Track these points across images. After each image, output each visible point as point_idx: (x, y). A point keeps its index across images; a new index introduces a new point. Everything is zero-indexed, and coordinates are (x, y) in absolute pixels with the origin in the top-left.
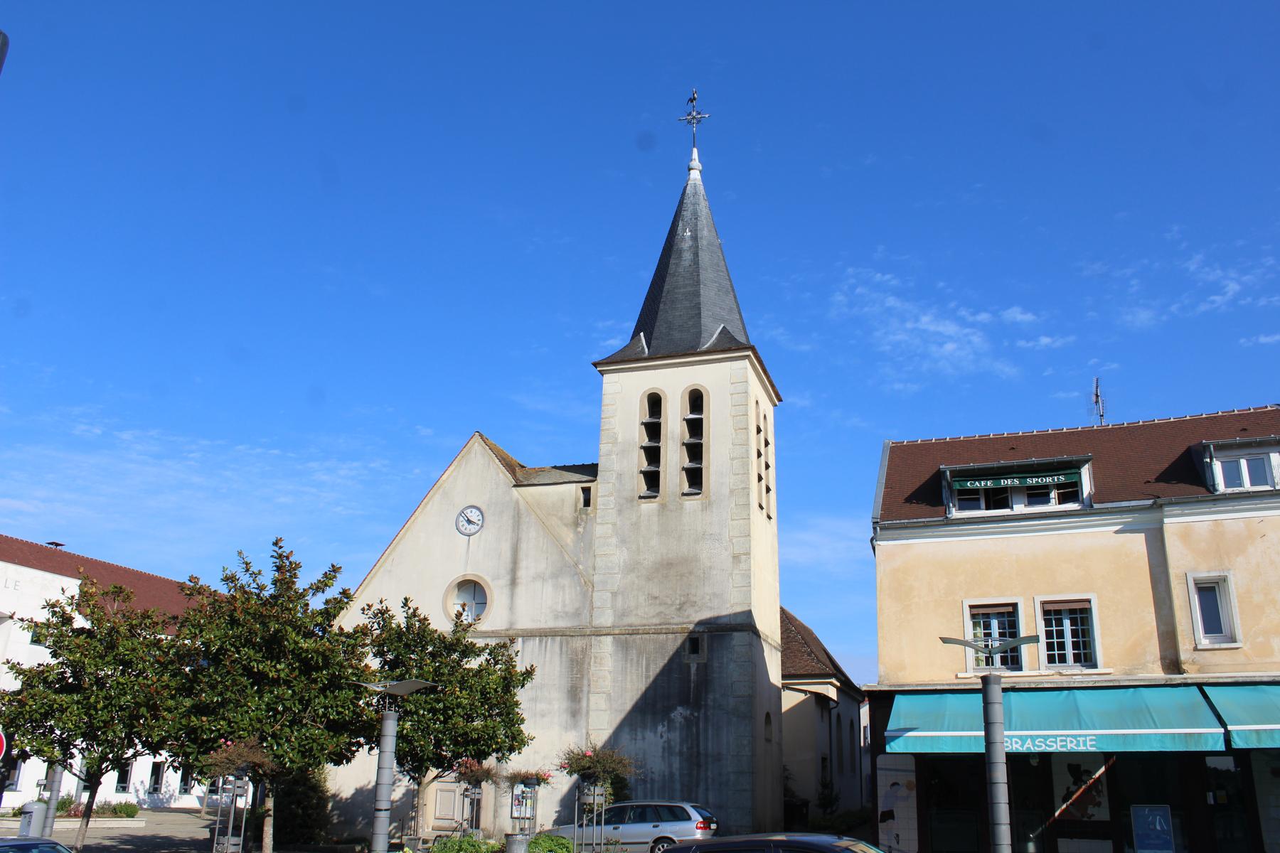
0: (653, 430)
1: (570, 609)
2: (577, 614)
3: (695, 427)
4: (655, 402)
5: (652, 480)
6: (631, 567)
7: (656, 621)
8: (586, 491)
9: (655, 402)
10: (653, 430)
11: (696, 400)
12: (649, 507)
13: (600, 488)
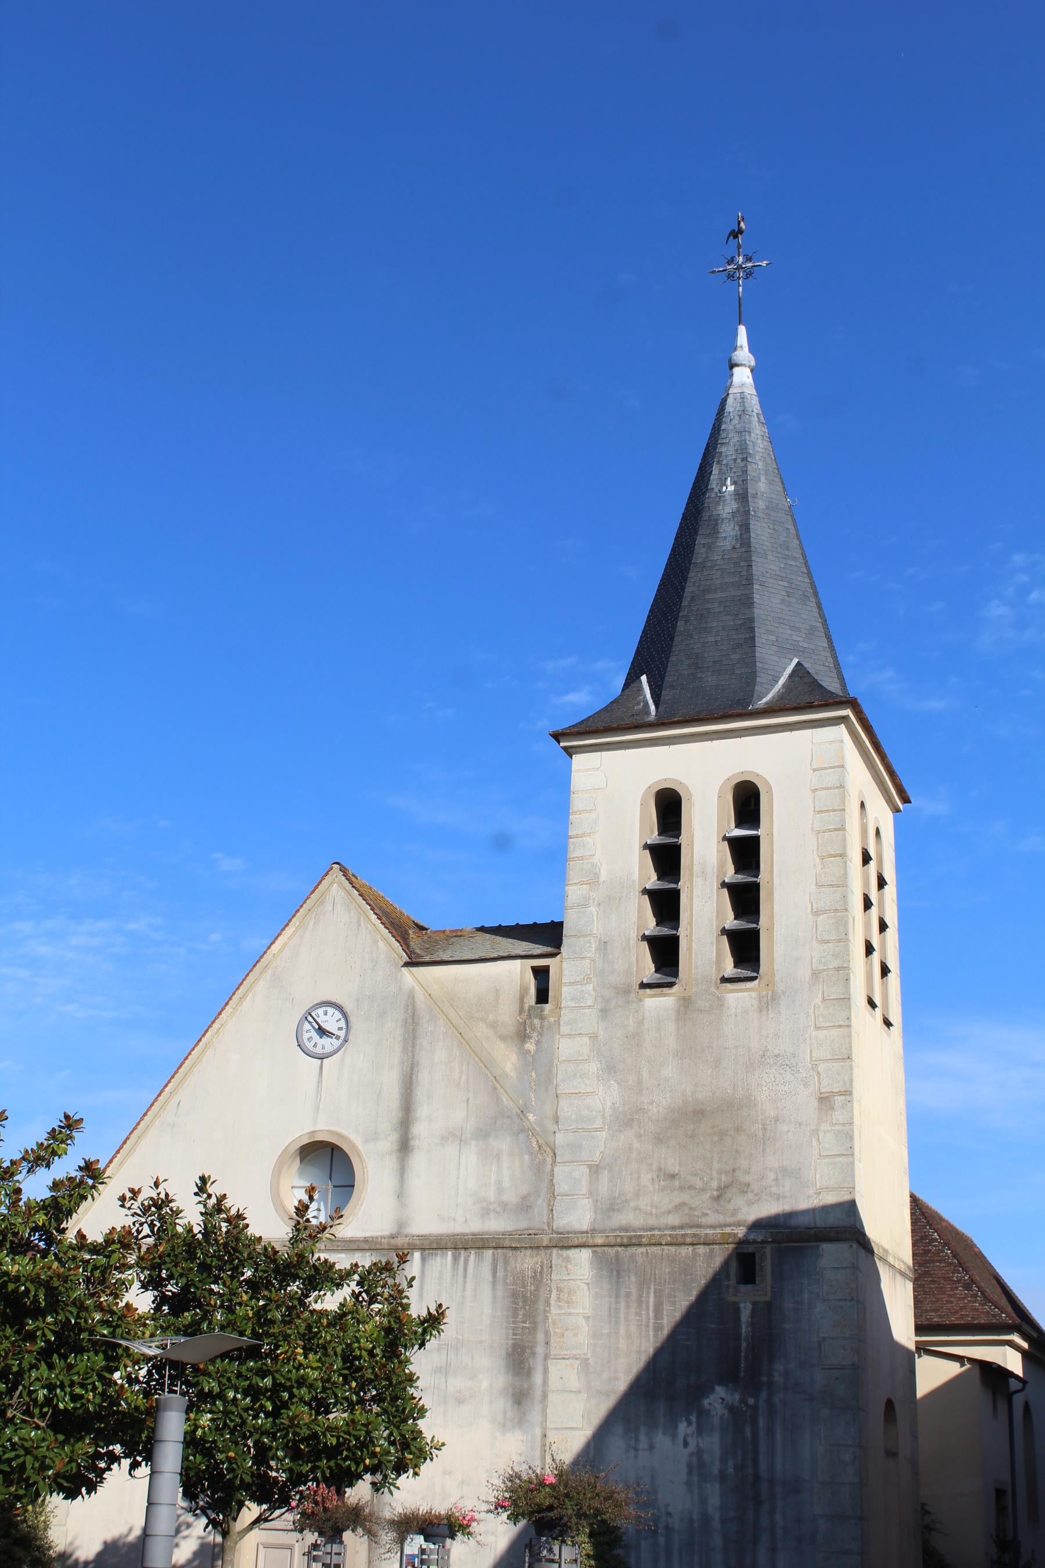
0: (667, 858)
1: (511, 1197)
2: (524, 1206)
3: (746, 853)
4: (669, 807)
5: (665, 952)
6: (626, 1119)
7: (673, 1220)
8: (541, 974)
9: (669, 807)
10: (667, 858)
11: (747, 802)
12: (659, 1004)
13: (565, 969)
